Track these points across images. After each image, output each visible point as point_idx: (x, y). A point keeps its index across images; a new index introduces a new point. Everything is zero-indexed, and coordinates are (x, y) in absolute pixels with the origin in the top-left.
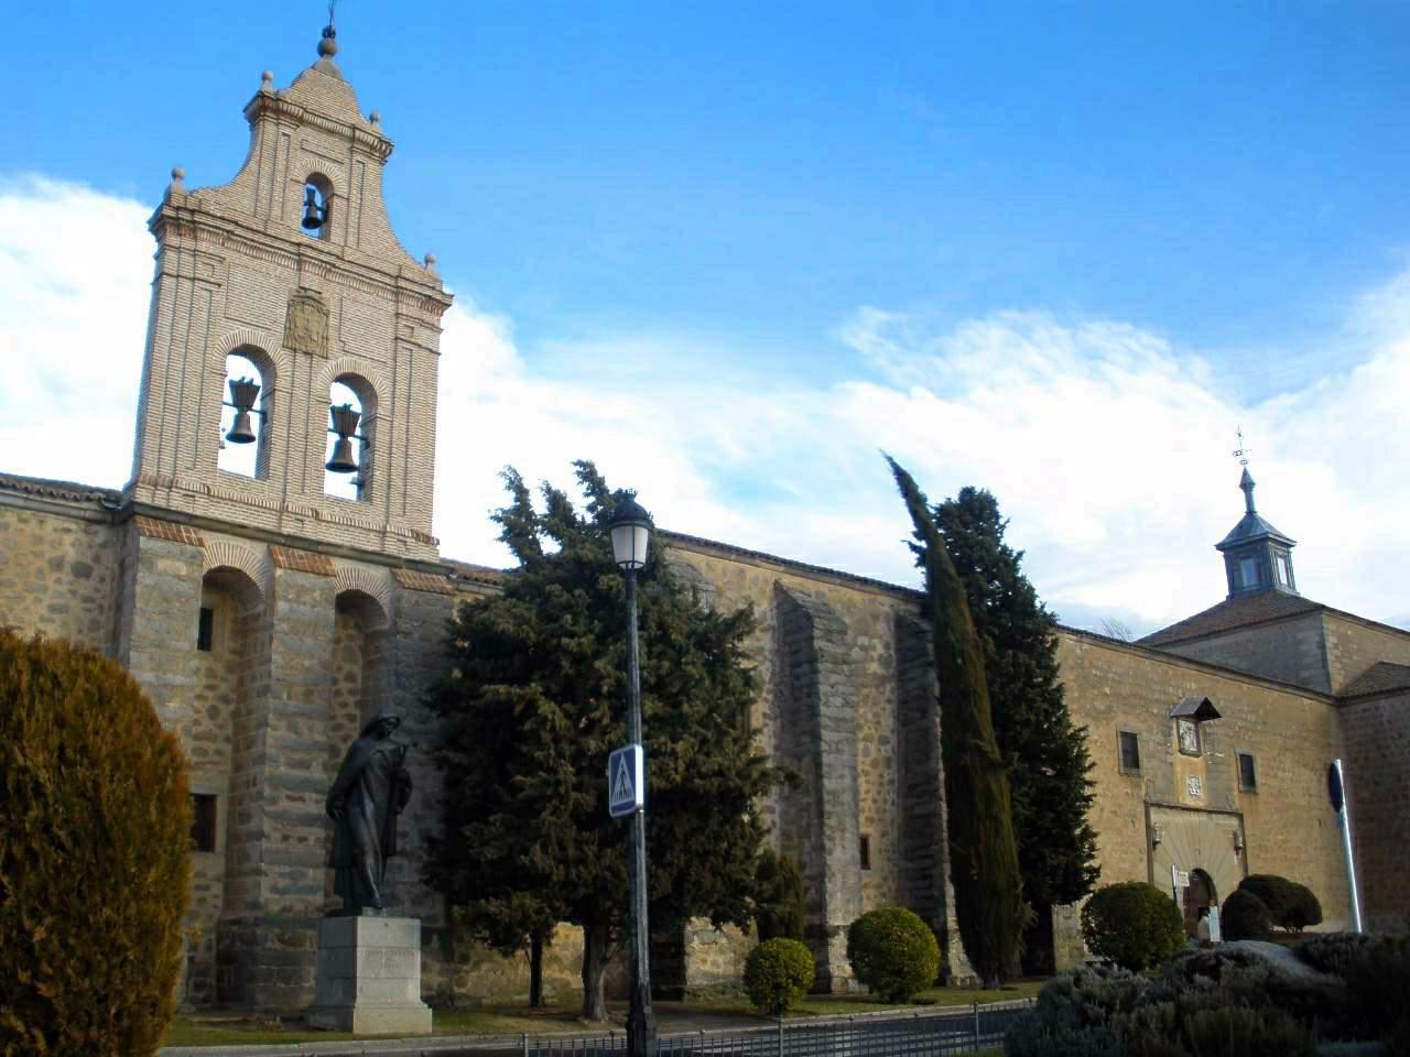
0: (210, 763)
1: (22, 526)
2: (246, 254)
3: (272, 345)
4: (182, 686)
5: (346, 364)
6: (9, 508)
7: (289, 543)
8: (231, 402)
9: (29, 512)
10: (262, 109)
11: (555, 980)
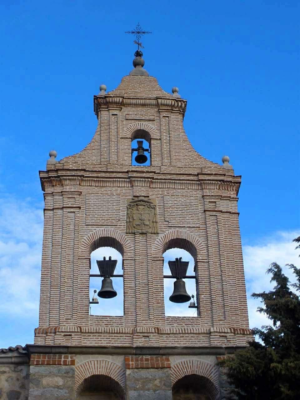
2: (96, 186)
3: (118, 234)
7: (138, 352)
8: (99, 273)
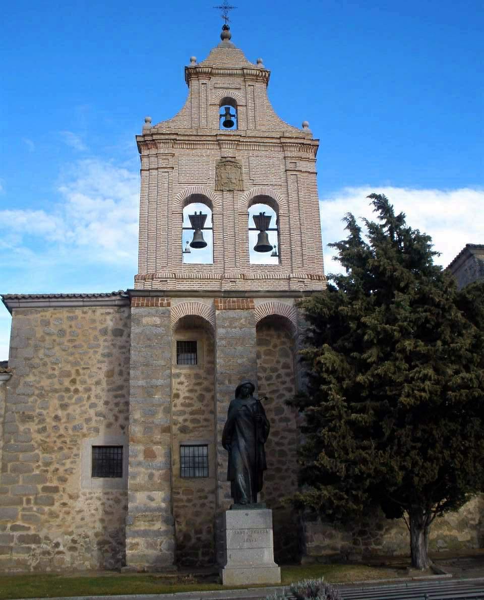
0: (202, 426)
1: (84, 315)
4: (162, 386)
5: (256, 191)
6: (76, 308)
7: (226, 295)
8: (254, 227)
9: (87, 308)
10: (191, 74)
11: (446, 536)
